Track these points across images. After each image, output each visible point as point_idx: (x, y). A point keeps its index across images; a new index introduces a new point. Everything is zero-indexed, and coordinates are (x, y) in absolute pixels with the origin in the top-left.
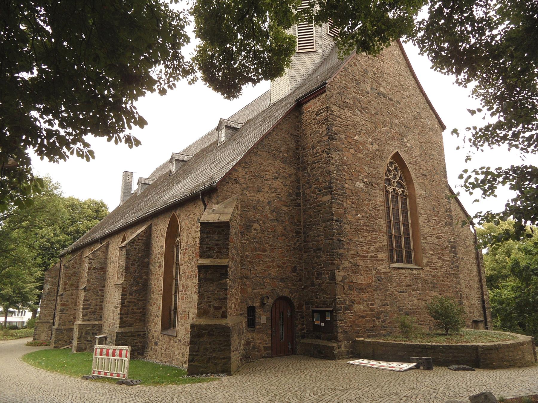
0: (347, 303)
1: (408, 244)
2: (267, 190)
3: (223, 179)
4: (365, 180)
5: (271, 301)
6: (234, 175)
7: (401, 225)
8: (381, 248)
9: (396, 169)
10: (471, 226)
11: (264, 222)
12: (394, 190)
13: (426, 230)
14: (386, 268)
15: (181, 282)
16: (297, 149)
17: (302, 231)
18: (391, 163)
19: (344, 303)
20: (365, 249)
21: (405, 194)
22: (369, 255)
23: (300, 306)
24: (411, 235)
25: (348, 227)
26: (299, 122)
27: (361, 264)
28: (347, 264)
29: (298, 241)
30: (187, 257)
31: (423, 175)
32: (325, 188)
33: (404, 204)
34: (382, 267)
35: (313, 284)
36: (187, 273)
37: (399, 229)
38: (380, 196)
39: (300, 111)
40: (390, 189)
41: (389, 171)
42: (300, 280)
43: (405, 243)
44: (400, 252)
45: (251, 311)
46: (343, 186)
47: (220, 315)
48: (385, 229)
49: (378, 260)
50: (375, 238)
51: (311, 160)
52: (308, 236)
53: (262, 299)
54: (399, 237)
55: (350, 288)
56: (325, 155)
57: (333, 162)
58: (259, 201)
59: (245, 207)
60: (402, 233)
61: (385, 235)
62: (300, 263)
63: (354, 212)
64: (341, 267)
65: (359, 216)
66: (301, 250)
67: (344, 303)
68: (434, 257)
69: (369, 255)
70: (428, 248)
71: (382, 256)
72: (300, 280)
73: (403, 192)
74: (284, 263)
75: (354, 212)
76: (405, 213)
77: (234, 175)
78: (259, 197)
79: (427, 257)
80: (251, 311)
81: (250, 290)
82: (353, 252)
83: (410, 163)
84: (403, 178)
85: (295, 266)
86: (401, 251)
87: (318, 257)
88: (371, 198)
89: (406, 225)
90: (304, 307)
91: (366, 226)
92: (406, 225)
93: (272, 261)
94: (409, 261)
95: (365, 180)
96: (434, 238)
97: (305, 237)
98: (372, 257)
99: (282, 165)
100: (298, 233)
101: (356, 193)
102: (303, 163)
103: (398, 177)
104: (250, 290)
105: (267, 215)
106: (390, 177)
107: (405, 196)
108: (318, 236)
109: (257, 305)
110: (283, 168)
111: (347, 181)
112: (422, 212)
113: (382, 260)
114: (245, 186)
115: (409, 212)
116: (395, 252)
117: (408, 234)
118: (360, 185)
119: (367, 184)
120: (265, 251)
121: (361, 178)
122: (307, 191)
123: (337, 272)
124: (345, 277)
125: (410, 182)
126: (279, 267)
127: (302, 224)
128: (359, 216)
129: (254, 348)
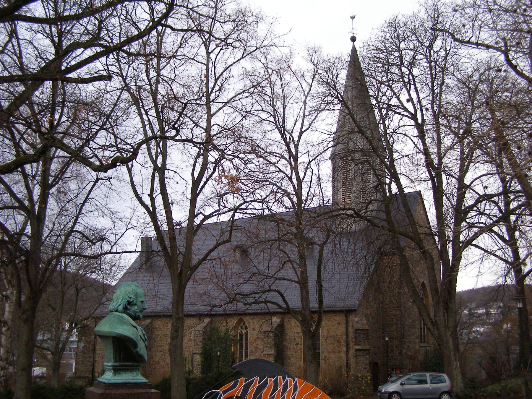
36: (329, 350)
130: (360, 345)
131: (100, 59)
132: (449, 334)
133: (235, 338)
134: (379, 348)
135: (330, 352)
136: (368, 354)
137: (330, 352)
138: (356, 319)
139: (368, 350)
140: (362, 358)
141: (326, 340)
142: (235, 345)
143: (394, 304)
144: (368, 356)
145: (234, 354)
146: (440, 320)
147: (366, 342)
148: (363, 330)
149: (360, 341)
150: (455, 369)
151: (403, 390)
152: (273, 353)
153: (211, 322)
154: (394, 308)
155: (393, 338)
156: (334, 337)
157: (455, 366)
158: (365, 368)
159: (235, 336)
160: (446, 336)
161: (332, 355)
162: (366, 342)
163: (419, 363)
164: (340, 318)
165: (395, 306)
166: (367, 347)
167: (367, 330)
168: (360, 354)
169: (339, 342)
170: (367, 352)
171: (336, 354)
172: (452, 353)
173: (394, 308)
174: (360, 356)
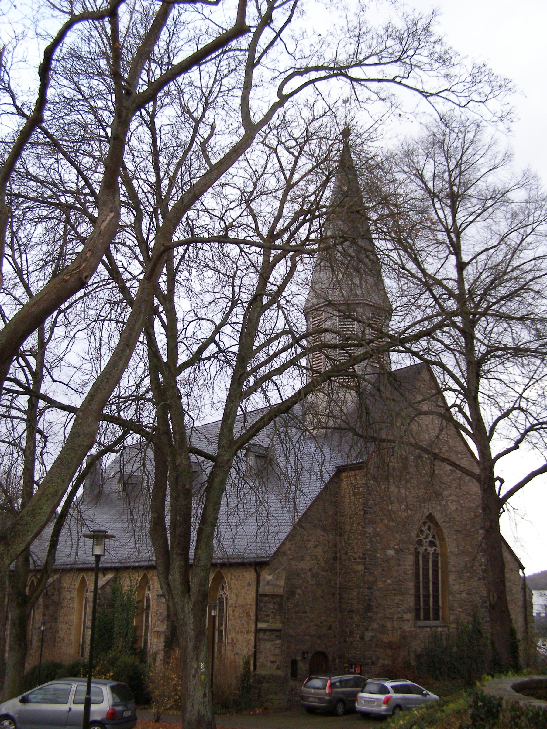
0: (374, 658)
1: (436, 601)
2: (308, 558)
3: (275, 553)
4: (396, 547)
5: (310, 655)
6: (283, 550)
7: (431, 584)
8: (407, 609)
9: (429, 529)
10: (521, 570)
11: (306, 587)
12: (426, 550)
13: (456, 588)
14: (411, 627)
15: (230, 636)
16: (336, 515)
17: (337, 592)
18: (424, 523)
19: (371, 658)
20: (392, 611)
21: (437, 552)
22: (396, 617)
23: (334, 660)
24: (440, 592)
25: (378, 593)
26: (338, 487)
27: (389, 625)
28: (375, 626)
29: (333, 602)
30: (237, 614)
31: (457, 531)
32: (359, 558)
33: (435, 563)
34: (407, 627)
35: (345, 641)
36: (237, 629)
37: (428, 587)
38: (410, 560)
39: (339, 477)
40: (422, 550)
41: (422, 532)
42: (335, 637)
43: (434, 602)
44: (426, 611)
45: (294, 663)
46: (375, 556)
47: (275, 668)
48: (412, 591)
49: (404, 621)
50: (402, 601)
51: (348, 528)
52: (343, 598)
53: (304, 653)
54: (426, 597)
55: (376, 646)
56: (360, 528)
57: (368, 535)
58: (302, 569)
59: (292, 575)
60: (431, 591)
61: (412, 597)
62: (335, 622)
63: (383, 579)
64: (370, 629)
65: (389, 581)
66: (336, 609)
67: (371, 658)
68: (462, 614)
69: (396, 617)
70: (456, 605)
71: (409, 616)
72: (335, 637)
73: (435, 550)
74: (321, 622)
75: (383, 579)
76: (435, 571)
77: (283, 550)
78: (303, 565)
79: (454, 614)
80: (294, 663)
81: (293, 646)
82: (381, 615)
83: (444, 522)
84: (436, 536)
85: (331, 625)
86: (429, 609)
87: (351, 618)
88: (401, 563)
89: (436, 584)
90: (337, 660)
91: (395, 590)
92: (436, 584)
93: (312, 621)
94: (436, 617)
95: (396, 547)
96: (464, 595)
97: (340, 599)
98: (398, 618)
99: (322, 533)
100: (333, 594)
101: (387, 561)
102: (341, 529)
103: (431, 536)
104: (293, 646)
105: (308, 581)
106: (422, 537)
107: (438, 554)
108: (352, 599)
109: (299, 658)
110: (323, 536)
111: (379, 551)
112: (453, 569)
113: (408, 620)
114: (291, 557)
115: (440, 571)
116: (422, 611)
117: (438, 591)
118: (391, 553)
119: (397, 551)
120: (305, 612)
121: (392, 546)
122: (344, 557)
123: (366, 633)
124: (373, 637)
125: (442, 539)
126: (317, 626)
127: (338, 586)
128: (389, 581)
129: (296, 694)
130: (267, 621)
131: (242, 128)
132: (189, 607)
133: (140, 605)
134: (330, 628)
135: (238, 632)
136: (279, 637)
137: (238, 632)
138: (269, 578)
139: (279, 631)
140: (268, 645)
141: (233, 611)
142: (140, 615)
143: (355, 553)
144: (278, 642)
145: (136, 629)
146: (174, 580)
147: (278, 617)
148: (273, 596)
149: (267, 615)
150: (194, 676)
151: (20, 712)
152: (163, 630)
153: (115, 580)
154: (355, 559)
155: (353, 611)
156: (243, 606)
157: (193, 671)
158: (272, 662)
159: (138, 602)
160: (183, 611)
161: (239, 637)
162: (278, 617)
163: (412, 655)
164: (250, 575)
165: (356, 556)
166: (278, 625)
167: (281, 596)
168: (266, 637)
169: (248, 614)
170: (278, 634)
171: (245, 636)
172: (191, 645)
173: (355, 559)
174: (265, 640)
